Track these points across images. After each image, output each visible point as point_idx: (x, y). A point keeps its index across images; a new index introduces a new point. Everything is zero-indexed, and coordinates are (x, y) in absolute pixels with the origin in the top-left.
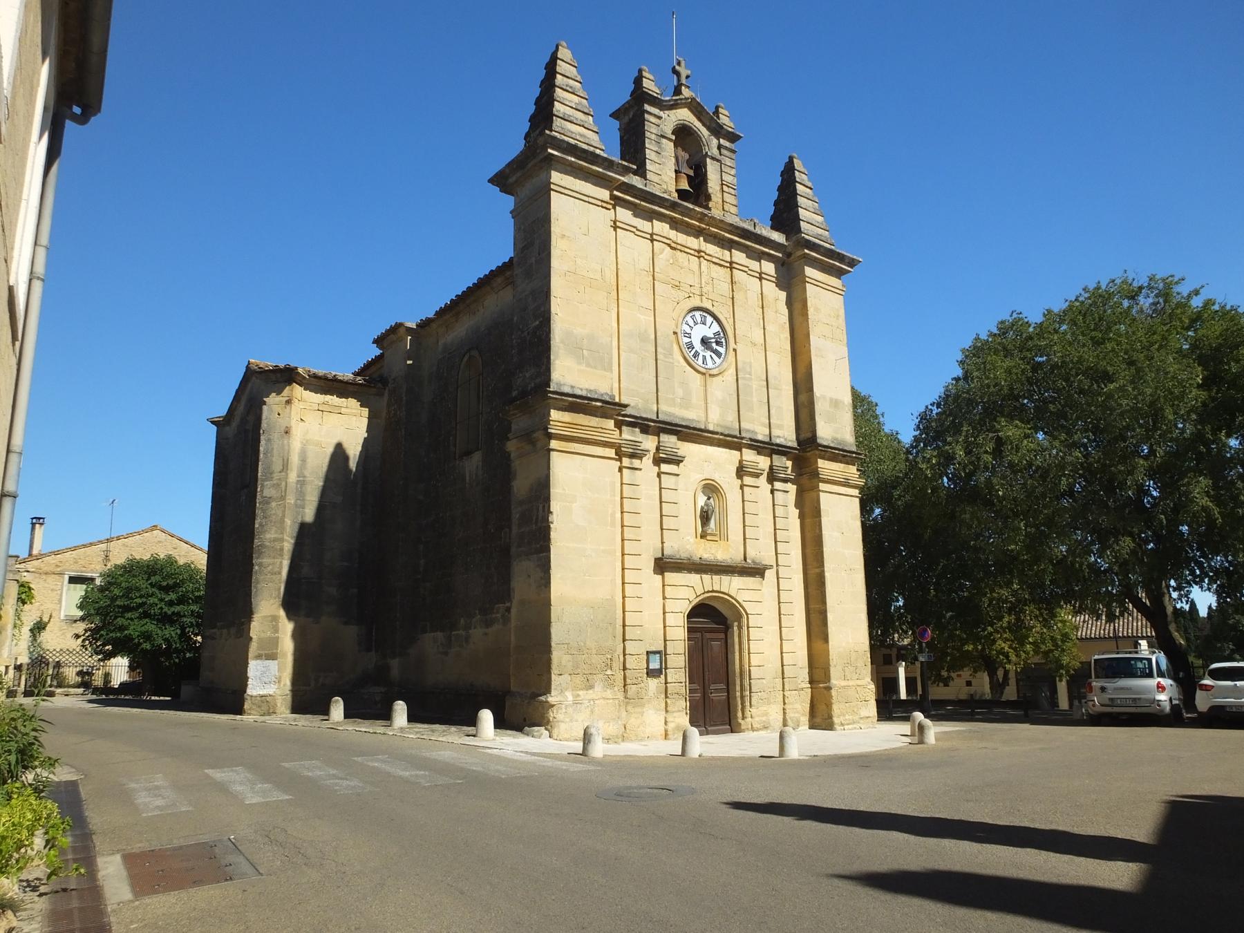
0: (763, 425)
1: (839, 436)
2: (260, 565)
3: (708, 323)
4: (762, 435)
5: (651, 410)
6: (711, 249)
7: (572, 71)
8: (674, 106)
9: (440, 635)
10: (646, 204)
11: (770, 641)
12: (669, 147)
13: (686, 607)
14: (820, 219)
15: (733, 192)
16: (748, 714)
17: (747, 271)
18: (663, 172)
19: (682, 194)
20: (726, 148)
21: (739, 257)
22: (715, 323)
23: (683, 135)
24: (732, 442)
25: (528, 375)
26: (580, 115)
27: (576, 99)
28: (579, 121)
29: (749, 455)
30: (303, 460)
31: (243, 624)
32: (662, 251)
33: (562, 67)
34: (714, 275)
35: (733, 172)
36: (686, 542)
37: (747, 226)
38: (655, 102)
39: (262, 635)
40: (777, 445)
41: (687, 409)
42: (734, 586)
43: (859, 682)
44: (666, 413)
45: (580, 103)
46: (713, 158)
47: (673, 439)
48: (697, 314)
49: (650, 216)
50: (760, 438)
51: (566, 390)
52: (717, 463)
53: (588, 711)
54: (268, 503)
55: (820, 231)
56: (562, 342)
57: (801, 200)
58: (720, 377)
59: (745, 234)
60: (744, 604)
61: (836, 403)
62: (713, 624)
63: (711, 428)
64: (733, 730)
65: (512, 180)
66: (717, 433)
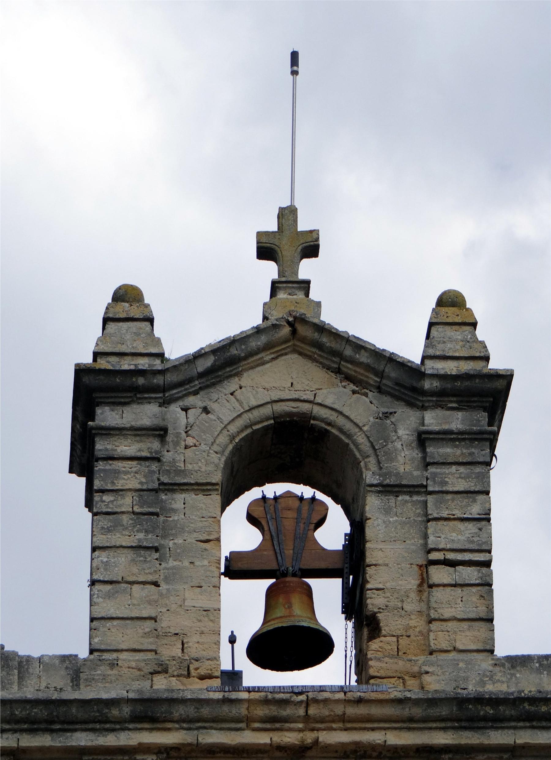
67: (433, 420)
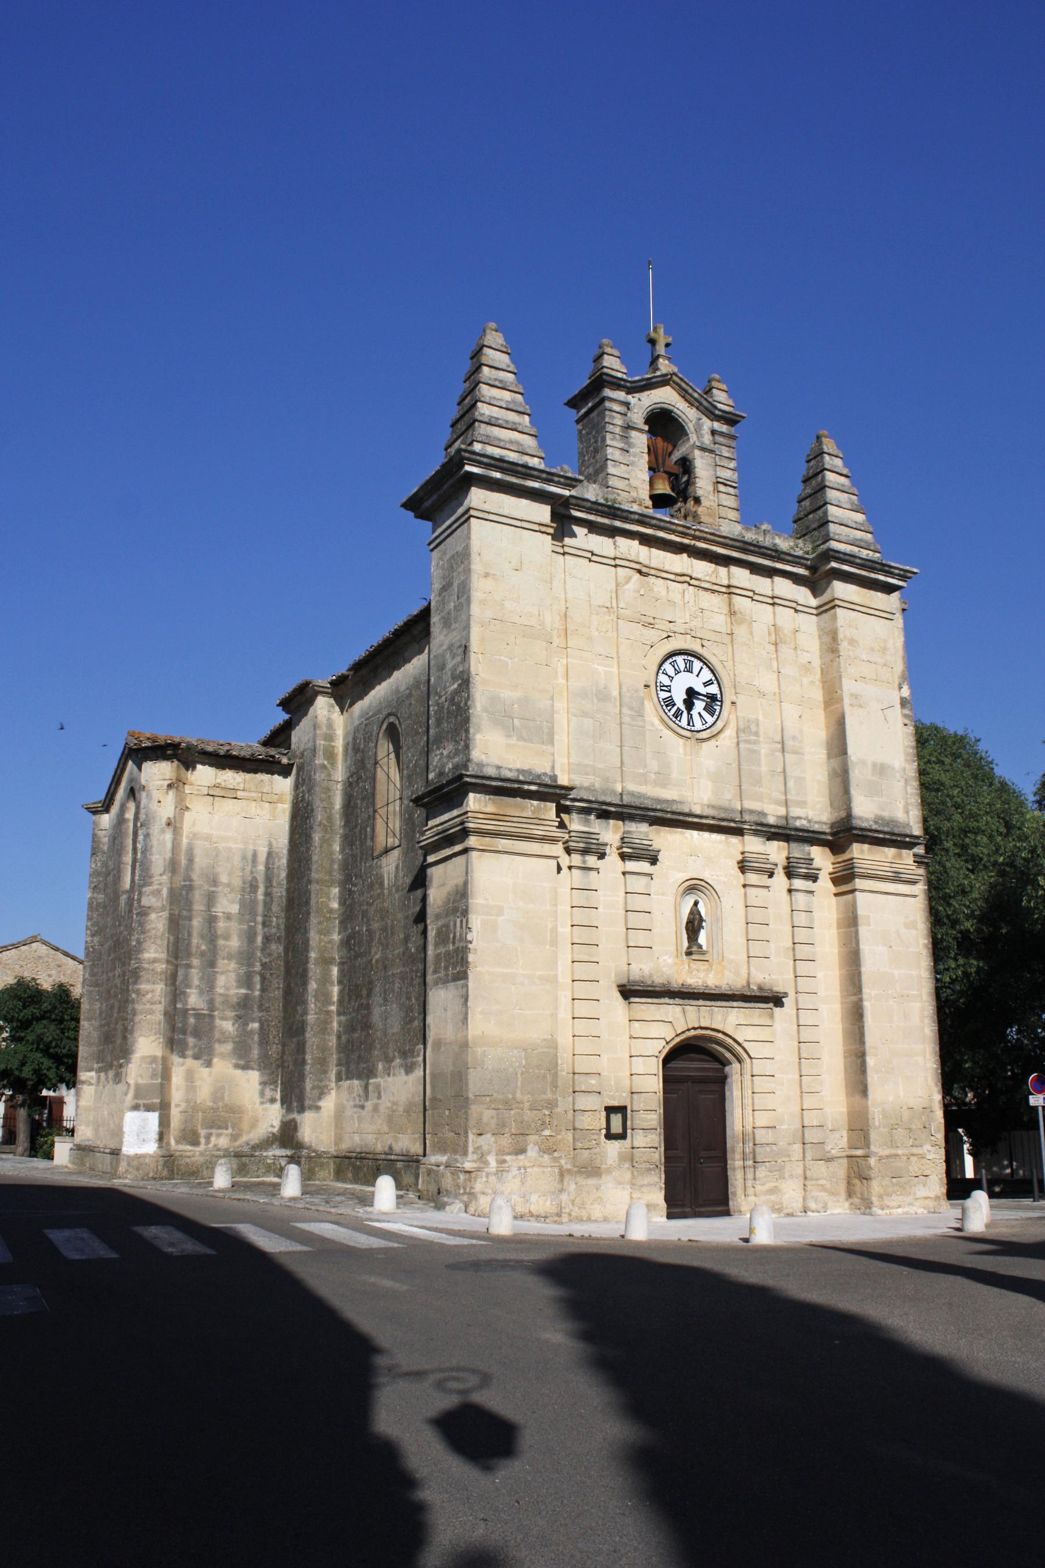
0: (777, 802)
1: (886, 814)
2: (138, 992)
3: (696, 670)
4: (774, 813)
5: (614, 792)
6: (702, 568)
7: (503, 360)
8: (648, 385)
9: (356, 1082)
10: (610, 520)
11: (778, 1090)
12: (640, 440)
13: (659, 1048)
14: (860, 517)
15: (731, 491)
16: (750, 1191)
17: (753, 596)
18: (631, 477)
19: (659, 501)
20: (721, 434)
21: (741, 576)
22: (705, 670)
23: (663, 425)
24: (728, 827)
25: (445, 753)
26: (512, 417)
27: (507, 395)
28: (507, 427)
29: (754, 844)
30: (191, 860)
31: (121, 1066)
32: (628, 580)
33: (491, 356)
34: (704, 605)
35: (733, 465)
36: (666, 964)
37: (750, 536)
38: (617, 384)
39: (140, 1081)
40: (797, 829)
41: (664, 786)
42: (731, 1022)
43: (915, 1150)
44: (632, 794)
45: (514, 401)
46: (703, 449)
47: (644, 827)
48: (680, 659)
49: (612, 532)
50: (771, 820)
51: (491, 772)
52: (710, 855)
53: (517, 1181)
54: (146, 914)
55: (859, 535)
56: (485, 710)
57: (831, 495)
58: (713, 742)
59: (746, 547)
60: (745, 1045)
61: (881, 769)
62: (697, 1073)
63: (697, 810)
64: (727, 1213)
65: (428, 503)
66: (707, 817)
67: (717, 425)
